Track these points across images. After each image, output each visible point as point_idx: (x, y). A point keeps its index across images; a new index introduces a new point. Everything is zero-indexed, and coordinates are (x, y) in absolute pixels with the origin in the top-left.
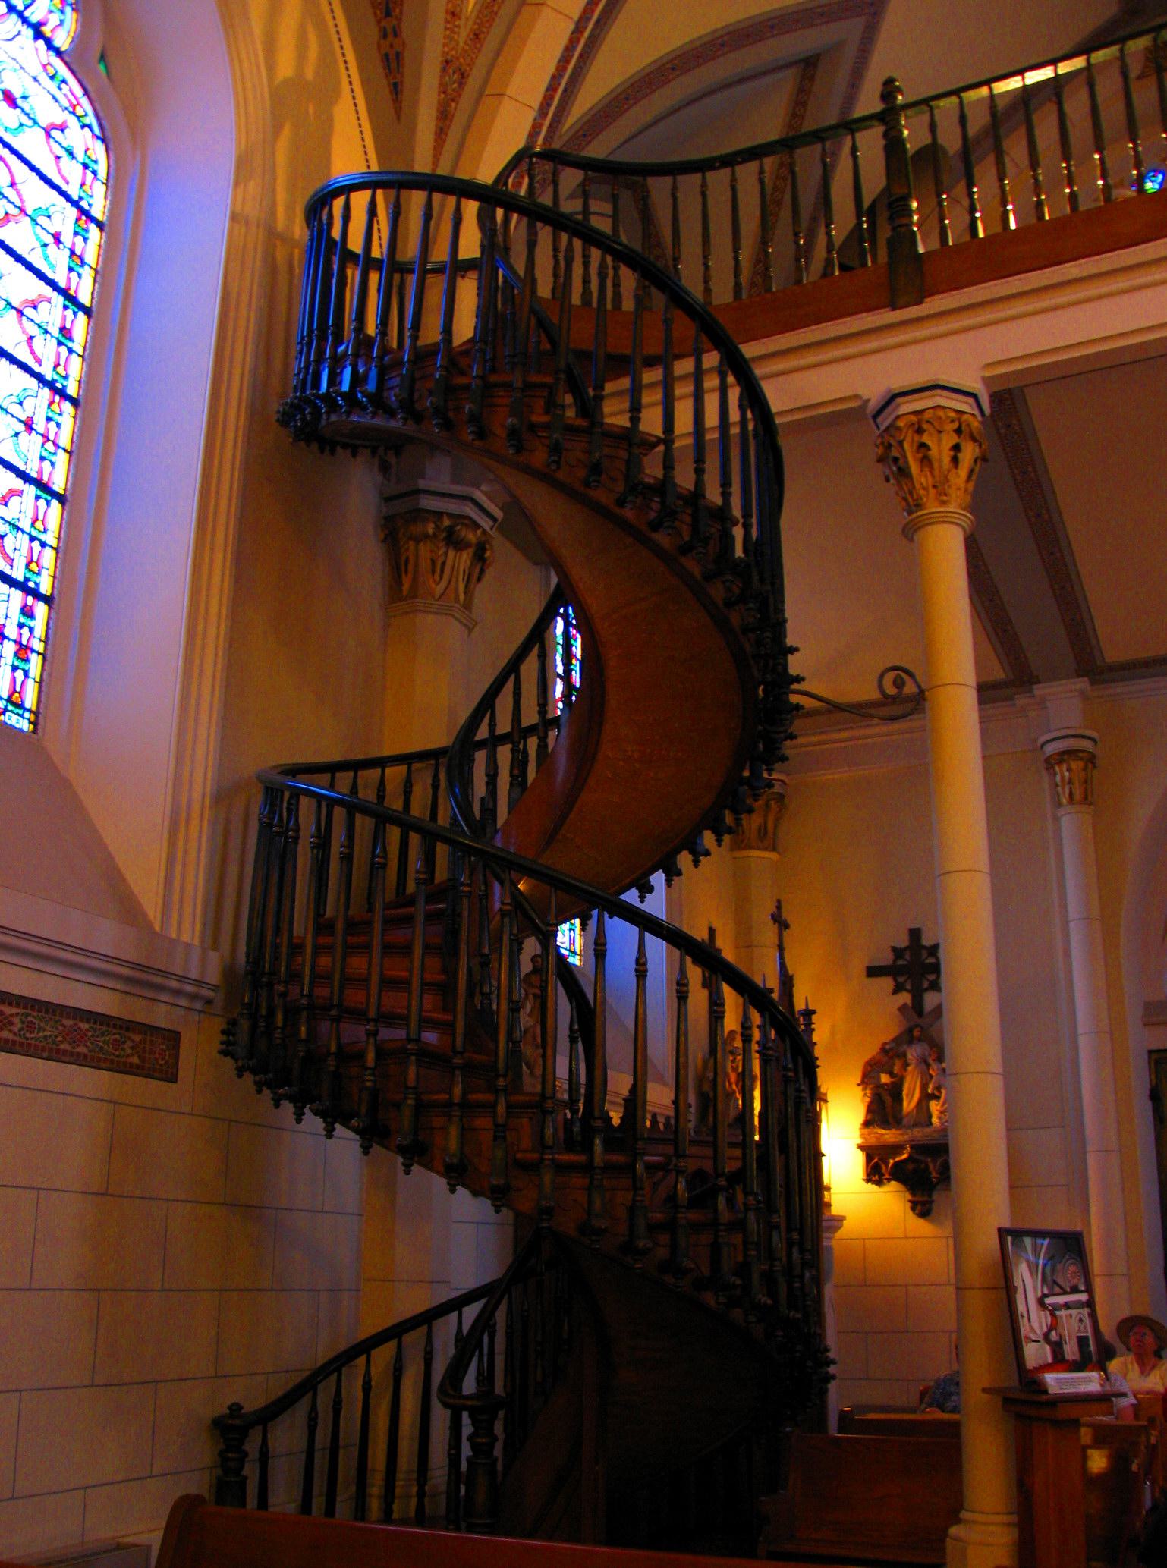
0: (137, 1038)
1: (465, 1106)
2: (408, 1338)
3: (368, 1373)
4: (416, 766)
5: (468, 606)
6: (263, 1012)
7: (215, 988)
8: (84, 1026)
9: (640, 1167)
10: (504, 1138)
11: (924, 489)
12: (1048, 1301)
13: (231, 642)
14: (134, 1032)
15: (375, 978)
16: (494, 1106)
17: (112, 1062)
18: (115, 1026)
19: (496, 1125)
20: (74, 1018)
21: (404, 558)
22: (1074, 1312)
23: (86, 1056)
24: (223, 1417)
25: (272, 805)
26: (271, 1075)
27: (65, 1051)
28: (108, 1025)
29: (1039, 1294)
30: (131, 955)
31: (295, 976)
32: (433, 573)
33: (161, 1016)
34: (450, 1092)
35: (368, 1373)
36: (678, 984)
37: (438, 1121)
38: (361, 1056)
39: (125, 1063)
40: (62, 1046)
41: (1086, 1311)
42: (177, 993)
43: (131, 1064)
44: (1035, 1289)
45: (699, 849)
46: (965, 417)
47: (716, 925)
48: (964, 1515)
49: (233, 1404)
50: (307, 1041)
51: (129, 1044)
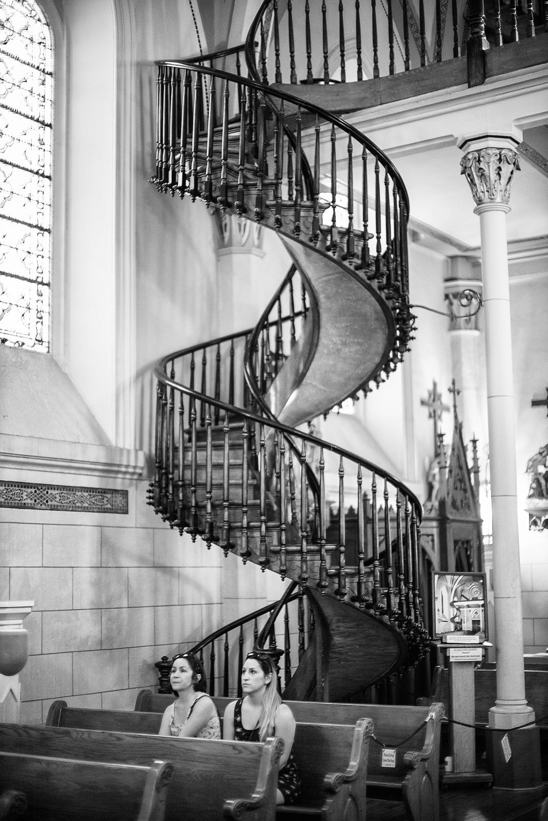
0: (109, 496)
1: (249, 528)
2: (245, 625)
3: (227, 642)
4: (235, 340)
5: (259, 247)
6: (164, 486)
7: (142, 468)
8: (86, 494)
9: (323, 551)
10: (265, 541)
11: (482, 192)
12: (455, 604)
13: (137, 318)
14: (107, 493)
15: (209, 469)
16: (260, 527)
17: (99, 508)
18: (99, 492)
19: (262, 536)
20: (81, 491)
21: (224, 223)
22: (472, 609)
23: (87, 507)
24: (160, 662)
25: (162, 390)
26: (168, 515)
27: (79, 507)
28: (96, 492)
29: (452, 601)
30: (103, 460)
31: (176, 467)
32: (240, 231)
33: (118, 484)
34: (242, 522)
35: (227, 642)
36: (340, 471)
37: (238, 534)
38: (205, 507)
39: (104, 508)
40: (77, 505)
41: (481, 609)
42: (126, 473)
43: (107, 508)
44: (449, 599)
45: (367, 389)
46: (503, 152)
47: (437, 380)
48: (497, 702)
49: (164, 657)
50: (182, 500)
51: (106, 499)
